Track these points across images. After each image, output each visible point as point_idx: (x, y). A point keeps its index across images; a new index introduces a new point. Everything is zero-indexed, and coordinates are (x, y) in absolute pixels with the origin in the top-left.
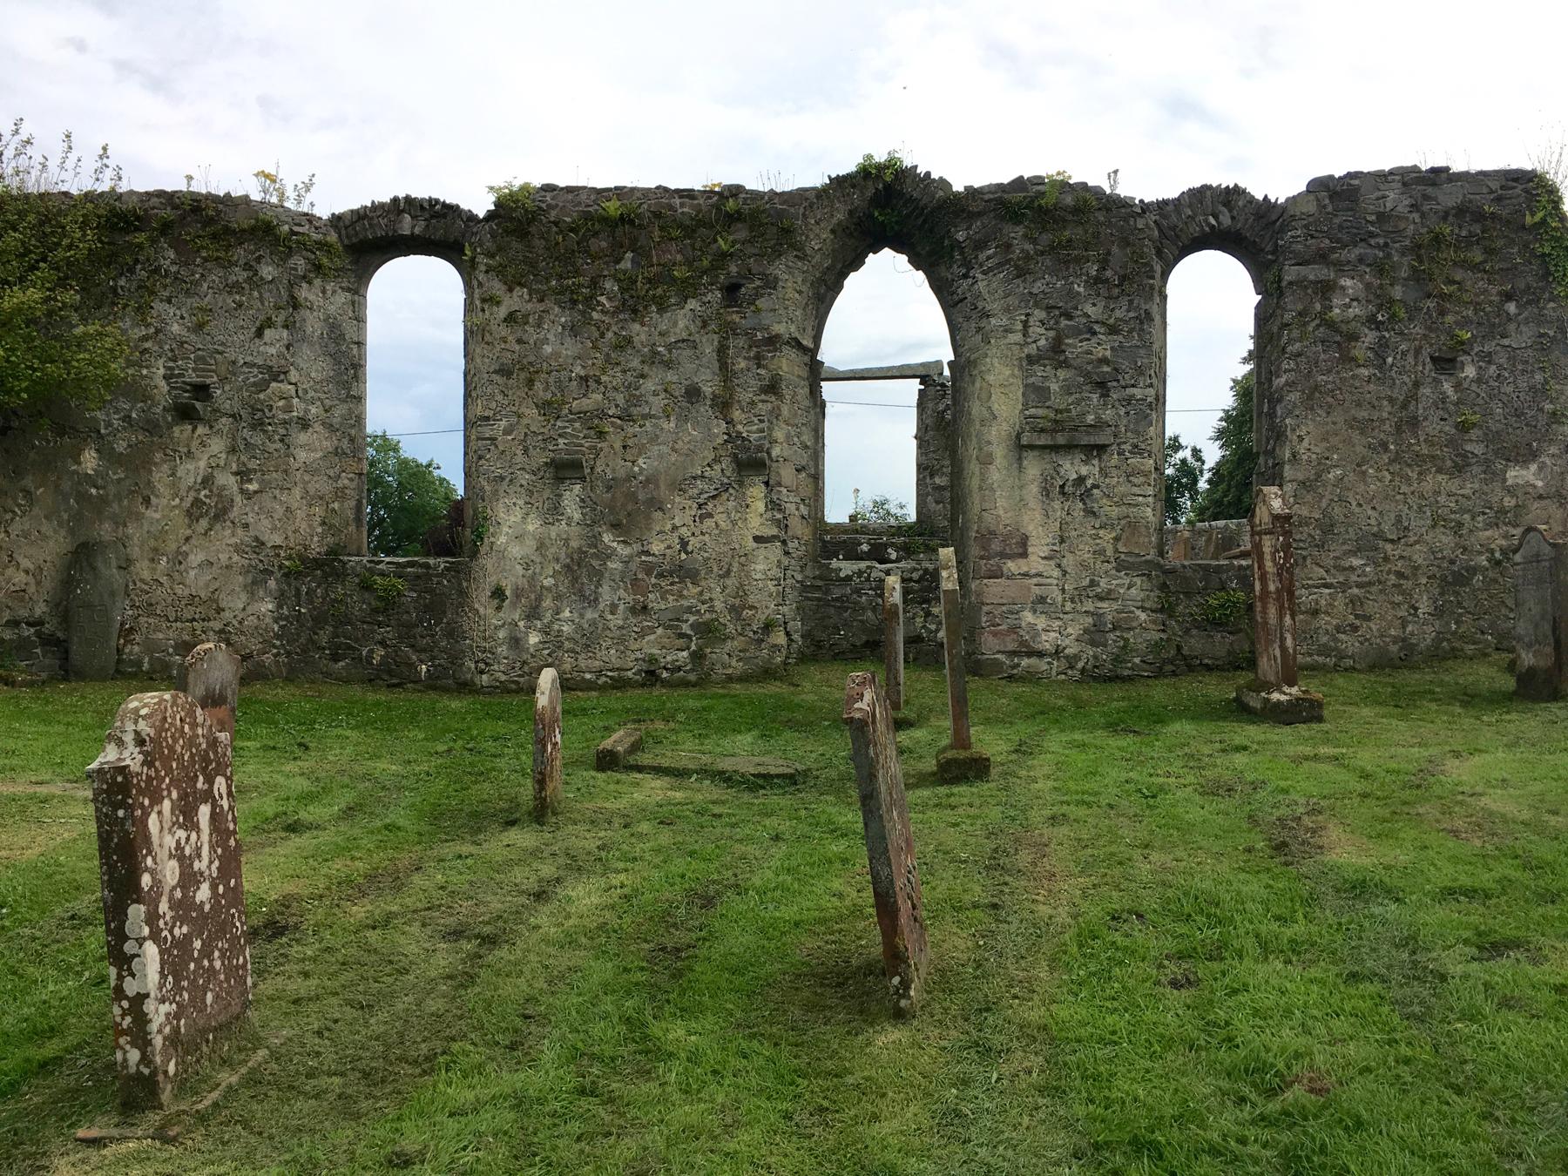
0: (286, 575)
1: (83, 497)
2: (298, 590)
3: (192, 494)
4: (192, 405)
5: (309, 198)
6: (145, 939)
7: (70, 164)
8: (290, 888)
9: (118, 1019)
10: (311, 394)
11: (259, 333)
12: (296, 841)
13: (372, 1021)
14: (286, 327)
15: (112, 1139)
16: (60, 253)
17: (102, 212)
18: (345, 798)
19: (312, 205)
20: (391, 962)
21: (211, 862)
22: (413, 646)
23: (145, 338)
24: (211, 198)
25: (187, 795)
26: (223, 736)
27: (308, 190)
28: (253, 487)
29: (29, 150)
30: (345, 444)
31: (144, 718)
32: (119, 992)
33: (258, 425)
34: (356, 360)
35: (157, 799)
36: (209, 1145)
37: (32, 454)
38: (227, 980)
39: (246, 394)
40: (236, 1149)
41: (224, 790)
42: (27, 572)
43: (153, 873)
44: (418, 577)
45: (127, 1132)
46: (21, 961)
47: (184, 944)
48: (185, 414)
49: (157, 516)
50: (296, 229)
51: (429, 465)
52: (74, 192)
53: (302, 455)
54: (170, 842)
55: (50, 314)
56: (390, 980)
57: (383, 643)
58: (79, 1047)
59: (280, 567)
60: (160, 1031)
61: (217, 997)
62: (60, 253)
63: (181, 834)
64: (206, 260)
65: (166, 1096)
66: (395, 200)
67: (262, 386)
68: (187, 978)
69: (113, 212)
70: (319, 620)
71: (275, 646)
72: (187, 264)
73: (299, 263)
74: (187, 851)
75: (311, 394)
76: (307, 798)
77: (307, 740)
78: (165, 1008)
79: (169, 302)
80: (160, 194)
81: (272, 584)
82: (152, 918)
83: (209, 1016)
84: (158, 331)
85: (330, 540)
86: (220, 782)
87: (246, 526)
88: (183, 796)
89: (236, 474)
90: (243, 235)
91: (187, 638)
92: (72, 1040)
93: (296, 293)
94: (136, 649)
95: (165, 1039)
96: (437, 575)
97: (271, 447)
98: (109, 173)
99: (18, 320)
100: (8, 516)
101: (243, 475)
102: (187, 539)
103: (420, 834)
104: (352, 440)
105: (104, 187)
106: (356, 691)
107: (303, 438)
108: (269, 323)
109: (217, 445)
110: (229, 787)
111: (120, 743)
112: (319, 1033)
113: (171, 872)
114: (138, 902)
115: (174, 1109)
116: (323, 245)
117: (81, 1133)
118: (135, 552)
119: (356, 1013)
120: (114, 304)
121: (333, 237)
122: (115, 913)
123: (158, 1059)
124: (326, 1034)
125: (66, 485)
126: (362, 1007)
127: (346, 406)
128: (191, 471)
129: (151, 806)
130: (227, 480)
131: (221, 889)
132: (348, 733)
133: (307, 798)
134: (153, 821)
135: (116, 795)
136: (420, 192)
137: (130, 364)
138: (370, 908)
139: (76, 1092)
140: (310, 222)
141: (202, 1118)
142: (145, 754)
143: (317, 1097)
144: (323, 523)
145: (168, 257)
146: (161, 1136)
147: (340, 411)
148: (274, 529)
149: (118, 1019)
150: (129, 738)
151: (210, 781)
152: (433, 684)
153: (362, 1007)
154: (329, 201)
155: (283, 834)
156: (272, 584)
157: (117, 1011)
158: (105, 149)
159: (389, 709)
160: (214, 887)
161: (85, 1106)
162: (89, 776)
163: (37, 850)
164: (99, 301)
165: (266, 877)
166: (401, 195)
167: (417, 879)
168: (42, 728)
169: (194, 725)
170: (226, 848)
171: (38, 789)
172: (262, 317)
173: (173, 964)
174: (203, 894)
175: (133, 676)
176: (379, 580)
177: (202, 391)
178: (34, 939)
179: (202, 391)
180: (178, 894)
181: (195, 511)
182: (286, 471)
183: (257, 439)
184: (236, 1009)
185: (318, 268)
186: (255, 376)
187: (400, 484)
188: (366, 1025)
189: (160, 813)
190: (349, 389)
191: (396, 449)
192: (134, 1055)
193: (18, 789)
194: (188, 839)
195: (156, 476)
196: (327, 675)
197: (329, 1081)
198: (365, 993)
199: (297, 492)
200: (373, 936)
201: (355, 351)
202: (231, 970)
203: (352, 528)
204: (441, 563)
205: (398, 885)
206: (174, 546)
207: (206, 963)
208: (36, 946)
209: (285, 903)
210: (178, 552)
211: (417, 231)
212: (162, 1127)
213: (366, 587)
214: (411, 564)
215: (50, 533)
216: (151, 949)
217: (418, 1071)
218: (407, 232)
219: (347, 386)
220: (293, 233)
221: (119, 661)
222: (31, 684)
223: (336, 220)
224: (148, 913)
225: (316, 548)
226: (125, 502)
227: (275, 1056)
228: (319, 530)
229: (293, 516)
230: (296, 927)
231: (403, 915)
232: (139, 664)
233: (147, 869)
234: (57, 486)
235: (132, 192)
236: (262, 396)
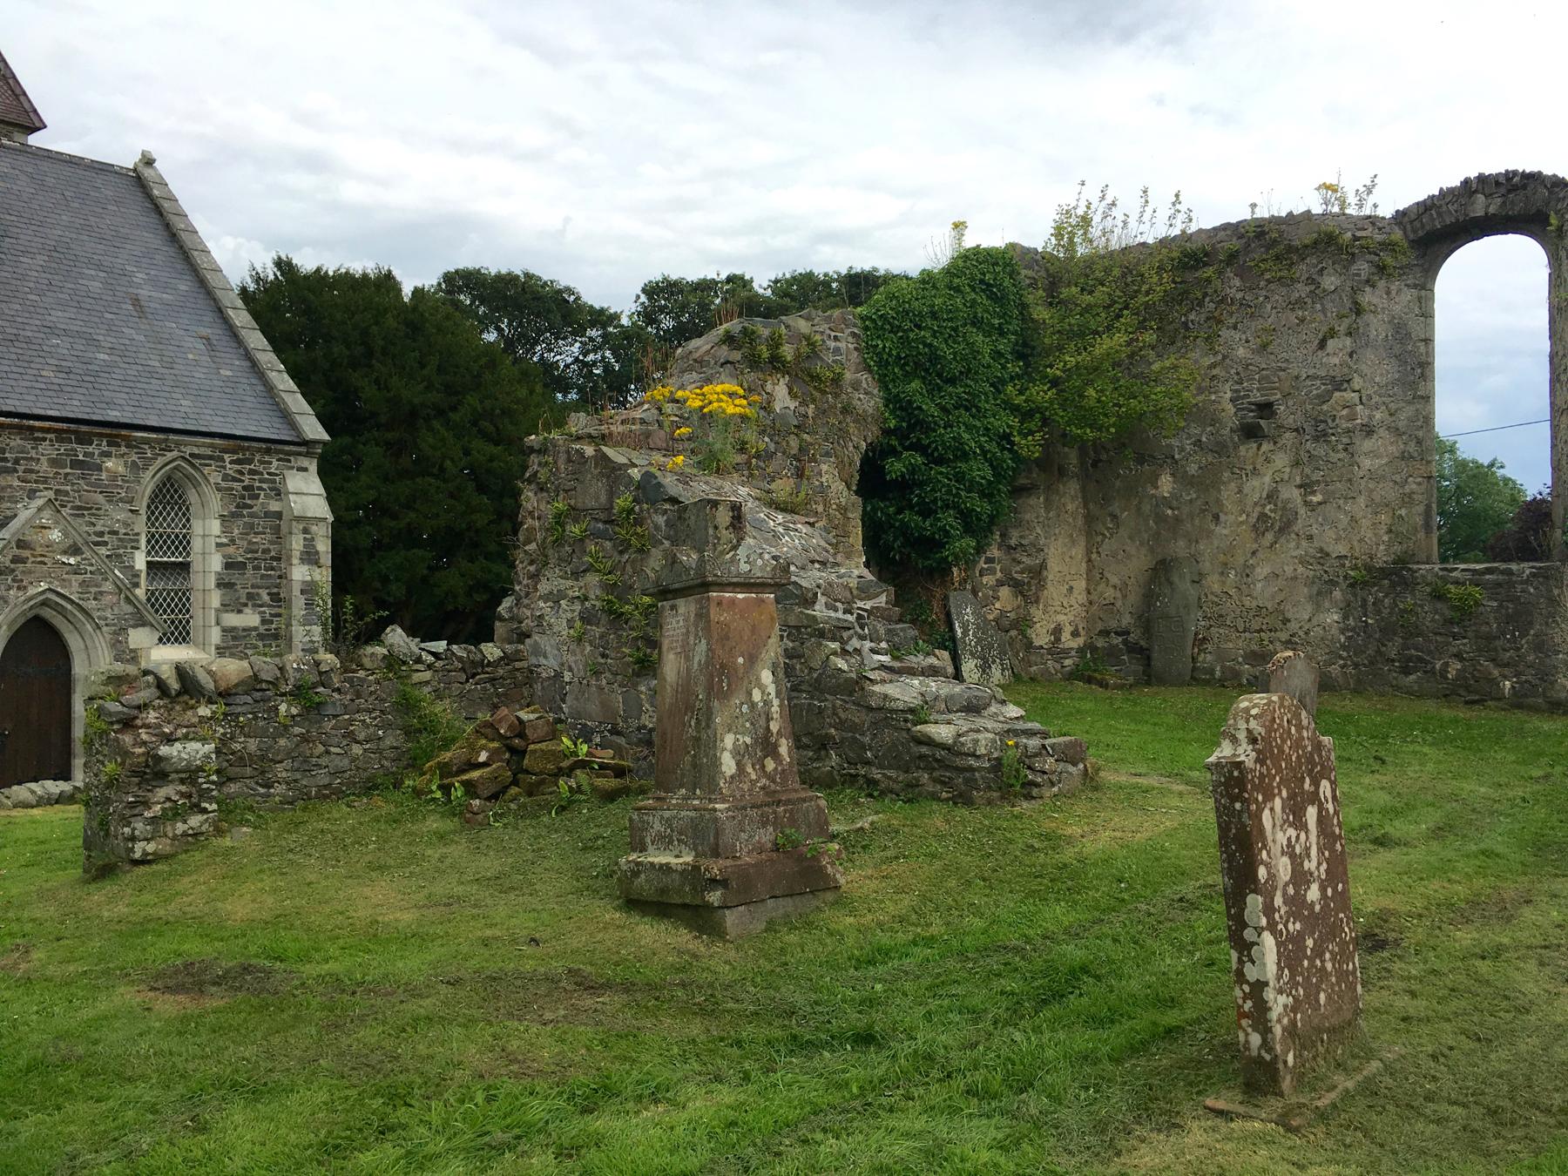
0: (1352, 585)
1: (1160, 519)
2: (1364, 601)
3: (1258, 509)
4: (1257, 424)
5: (1371, 200)
6: (1263, 929)
7: (1146, 217)
8: (1386, 902)
9: (1240, 1001)
10: (1376, 399)
11: (1322, 345)
12: (1386, 856)
13: (1493, 1056)
14: (1350, 334)
15: (1238, 1115)
16: (1142, 299)
17: (1175, 254)
18: (1431, 818)
19: (1375, 206)
20: (1507, 998)
21: (1319, 864)
22: (1493, 660)
23: (1213, 366)
24: (1274, 220)
25: (1296, 795)
26: (1326, 740)
27: (1370, 192)
28: (1316, 499)
29: (1115, 212)
30: (1412, 447)
31: (1255, 717)
32: (1240, 977)
33: (1321, 436)
34: (1423, 358)
35: (1269, 797)
36: (1329, 1144)
37: (1118, 483)
38: (1338, 983)
39: (1309, 407)
40: (1358, 1154)
41: (1329, 794)
42: (1115, 587)
43: (1268, 866)
44: (1499, 585)
45: (1252, 1111)
46: (1140, 933)
47: (1298, 939)
48: (1251, 432)
49: (1225, 532)
50: (1359, 234)
51: (1492, 465)
52: (1151, 241)
53: (1367, 463)
54: (1281, 838)
55: (1131, 356)
56: (1509, 1016)
57: (1458, 656)
58: (1198, 1021)
59: (1345, 577)
60: (1279, 1021)
61: (1329, 998)
62: (1142, 299)
63: (1292, 832)
64: (1269, 281)
65: (1286, 1084)
66: (1466, 182)
67: (1324, 398)
68: (1302, 974)
69: (1185, 254)
70: (1387, 631)
71: (1341, 657)
72: (1251, 289)
73: (1363, 267)
74: (1298, 851)
75: (1376, 399)
76: (1392, 813)
77: (1382, 754)
78: (1282, 999)
79: (1235, 328)
80: (1226, 227)
81: (1337, 594)
82: (1269, 910)
83: (1325, 1017)
84: (1225, 357)
85: (1397, 548)
86: (1325, 785)
87: (1310, 538)
88: (1292, 796)
89: (1300, 487)
90: (1302, 252)
91: (1255, 648)
92: (1190, 1014)
93: (1360, 298)
94: (1209, 657)
95: (1284, 1029)
96: (1522, 582)
97: (1334, 457)
98: (1181, 217)
99: (1106, 365)
100: (1099, 539)
101: (1307, 487)
102: (1254, 553)
103: (1523, 864)
104: (1419, 442)
105: (1176, 231)
106: (1430, 706)
107: (1368, 445)
108: (1332, 333)
109: (1281, 461)
110: (1334, 791)
111: (1235, 740)
112: (1434, 1057)
113: (1284, 867)
114: (1255, 891)
115: (1294, 1100)
116: (1389, 246)
117: (1210, 1102)
118: (1206, 566)
119: (1474, 1045)
120: (1185, 337)
121: (1397, 235)
122: (1235, 898)
123: (1278, 1048)
124: (1442, 1060)
125: (1146, 508)
126: (1479, 1040)
127: (1412, 408)
128: (1256, 487)
129: (1264, 802)
130: (1291, 494)
131: (1329, 891)
132: (1426, 749)
133: (1392, 813)
134: (1266, 815)
135: (1232, 787)
136: (1494, 167)
137: (1200, 390)
138: (1476, 935)
139: (1199, 1063)
140: (1373, 224)
141: (1322, 1116)
142: (1258, 752)
143: (1438, 1122)
144: (1390, 531)
145: (1233, 286)
146: (1283, 1121)
147: (1409, 411)
148: (1337, 540)
149: (1240, 1001)
150: (1242, 736)
151: (1316, 784)
152: (1518, 703)
153: (1479, 1040)
154: (1388, 203)
155: (1371, 847)
156: (1337, 594)
157: (1238, 993)
158: (1177, 196)
159: (1469, 728)
160: (1323, 889)
161: (1209, 1077)
162: (1208, 767)
163: (1146, 835)
164: (1174, 336)
165: (1373, 885)
166: (1473, 174)
167: (1527, 911)
168: (1133, 726)
169: (1300, 727)
170: (1333, 851)
171: (1140, 780)
172: (1325, 329)
173: (1288, 958)
174: (1313, 894)
175: (1207, 683)
176: (1452, 588)
177: (1266, 409)
178: (1150, 915)
179: (1266, 409)
180: (1291, 891)
181: (1261, 524)
182: (1350, 480)
183: (1320, 450)
184: (1348, 1016)
185: (1381, 269)
186: (1318, 388)
187: (1458, 487)
188: (1485, 1057)
189: (1272, 809)
190: (1417, 389)
191: (1452, 450)
192: (1256, 1039)
193: (1123, 779)
194: (1298, 837)
195: (1225, 494)
196: (1397, 688)
197: (1451, 1109)
198: (1481, 1024)
199: (1362, 501)
200: (1484, 967)
201: (1422, 349)
202: (1342, 975)
203: (1421, 535)
204: (1525, 568)
205: (1506, 916)
206: (1242, 561)
207: (1318, 963)
208: (1152, 920)
209: (1383, 916)
210: (1245, 566)
211: (1492, 210)
212: (1285, 1115)
213: (1438, 596)
214: (1489, 571)
215: (1133, 552)
216: (1268, 940)
217: (1552, 1121)
218: (1480, 213)
219: (1413, 385)
220: (1356, 239)
221: (1194, 669)
222: (1121, 687)
223: (1401, 216)
224: (1264, 903)
225: (1382, 557)
226: (1197, 522)
227: (1389, 1069)
228: (1386, 538)
229: (1358, 527)
230: (1397, 943)
231: (1516, 949)
232: (1212, 671)
233: (1262, 862)
234: (1139, 509)
235: (1200, 231)
236: (1325, 407)
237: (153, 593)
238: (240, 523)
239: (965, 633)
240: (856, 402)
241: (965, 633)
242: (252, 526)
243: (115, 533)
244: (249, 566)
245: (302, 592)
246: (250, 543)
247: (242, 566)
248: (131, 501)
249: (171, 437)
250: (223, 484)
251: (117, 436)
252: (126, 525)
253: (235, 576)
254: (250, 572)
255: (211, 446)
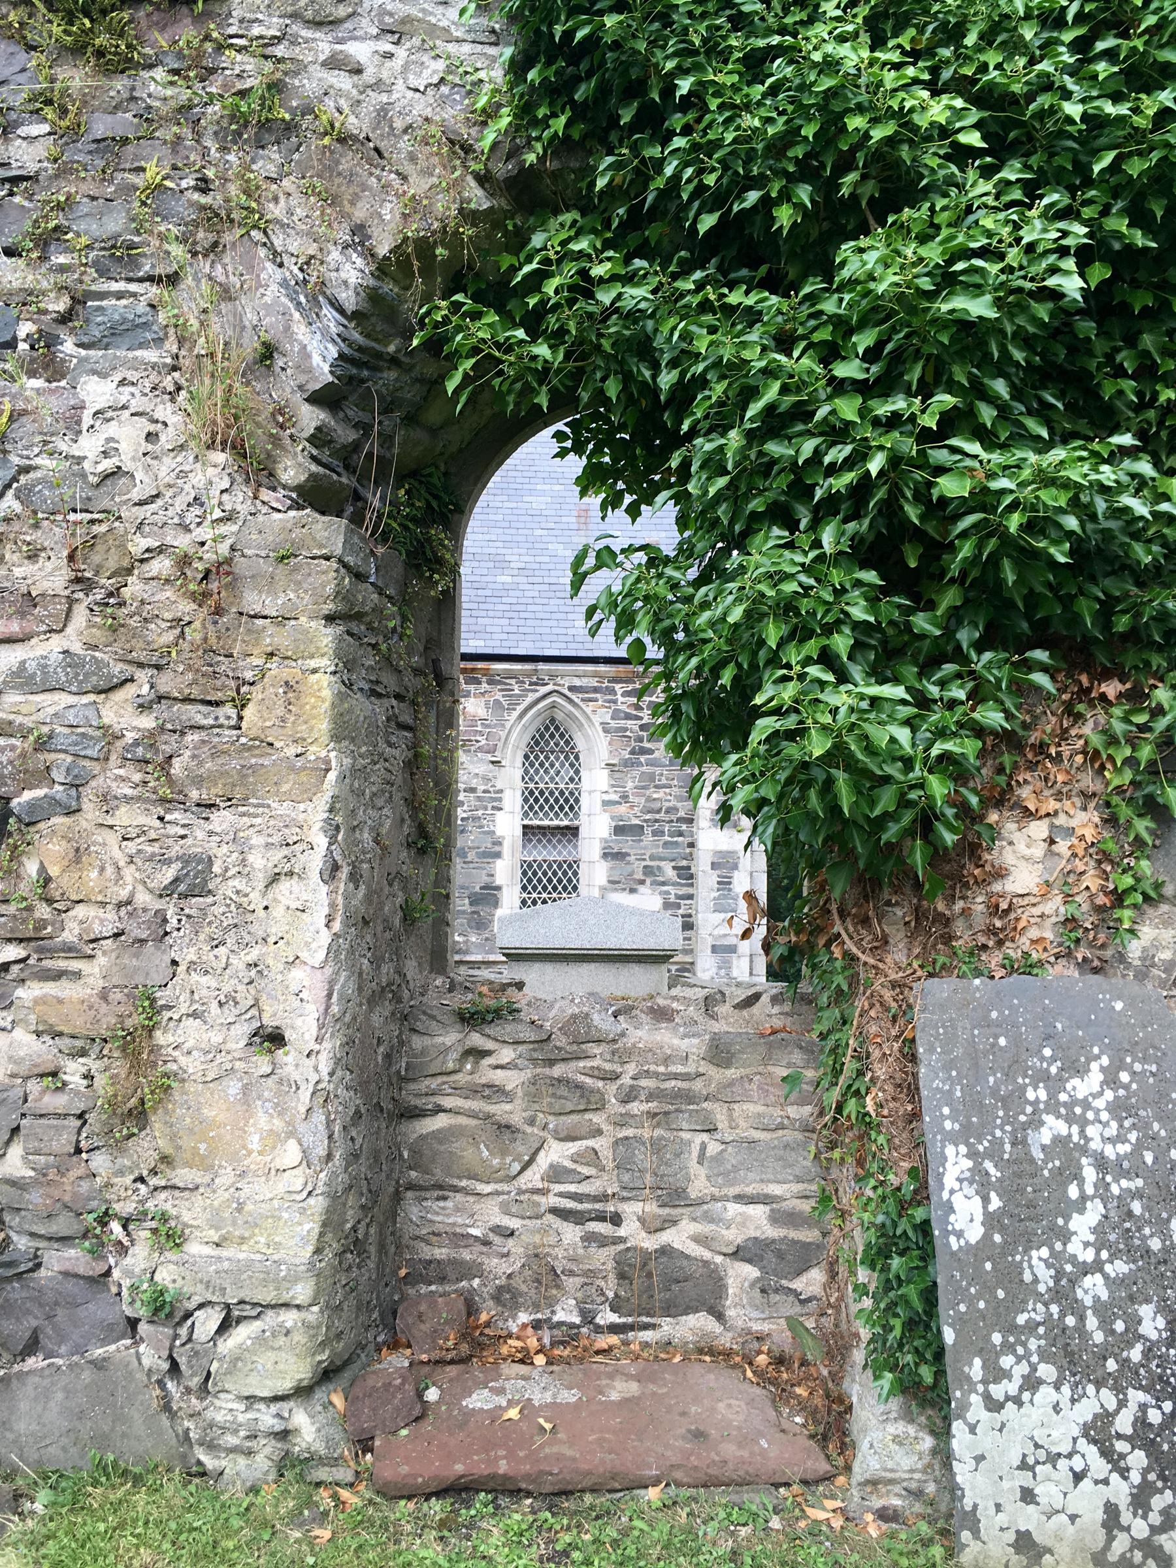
237: (530, 866)
238: (636, 773)
239: (1030, 1207)
240: (310, 84)
241: (1030, 1207)
242: (652, 777)
243: (473, 790)
244: (648, 831)
245: (714, 866)
246: (650, 799)
247: (638, 830)
248: (492, 750)
249: (541, 666)
250: (613, 724)
251: (473, 670)
252: (487, 780)
253: (626, 844)
254: (648, 838)
255: (595, 675)
